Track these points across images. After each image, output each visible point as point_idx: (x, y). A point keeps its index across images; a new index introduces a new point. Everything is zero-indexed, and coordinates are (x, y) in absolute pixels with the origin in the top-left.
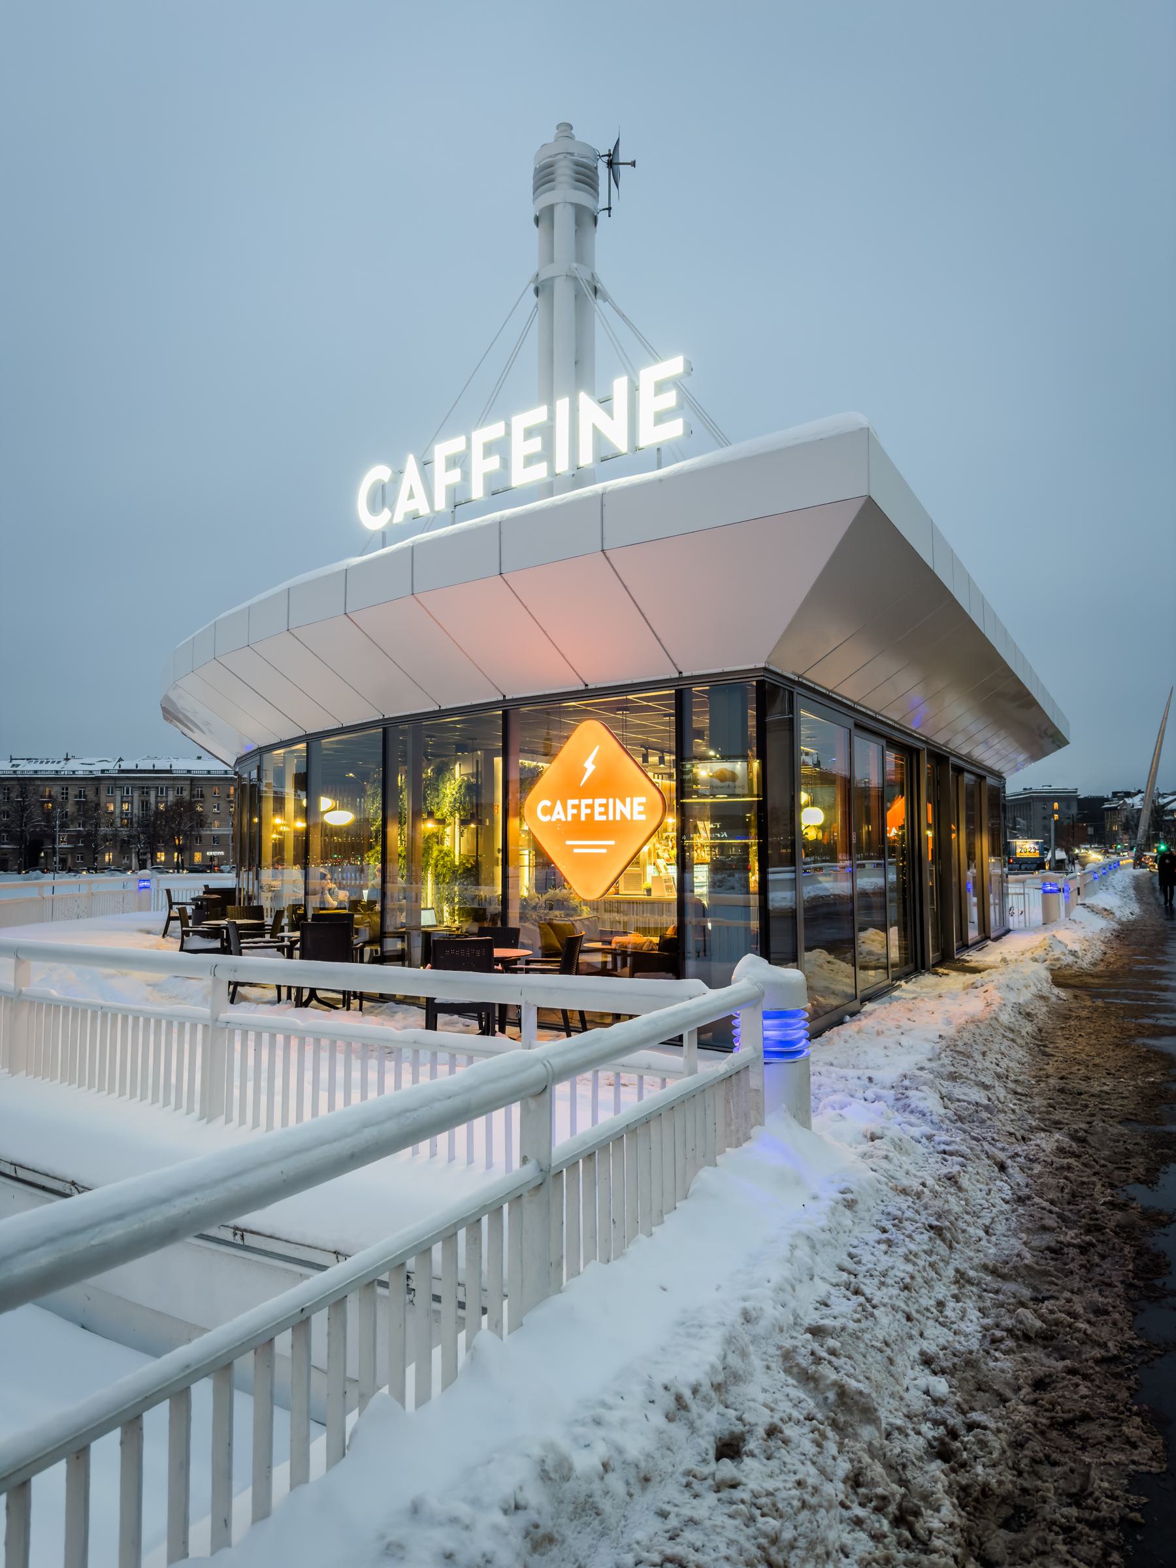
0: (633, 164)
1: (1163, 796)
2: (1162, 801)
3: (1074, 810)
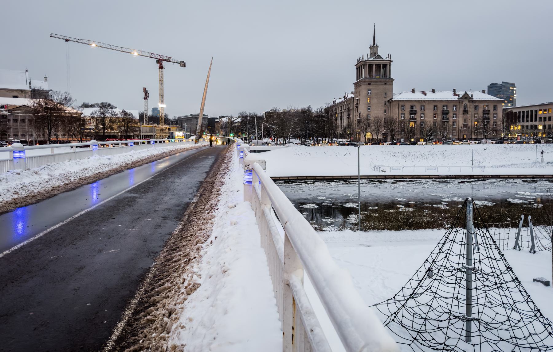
0: (183, 64)
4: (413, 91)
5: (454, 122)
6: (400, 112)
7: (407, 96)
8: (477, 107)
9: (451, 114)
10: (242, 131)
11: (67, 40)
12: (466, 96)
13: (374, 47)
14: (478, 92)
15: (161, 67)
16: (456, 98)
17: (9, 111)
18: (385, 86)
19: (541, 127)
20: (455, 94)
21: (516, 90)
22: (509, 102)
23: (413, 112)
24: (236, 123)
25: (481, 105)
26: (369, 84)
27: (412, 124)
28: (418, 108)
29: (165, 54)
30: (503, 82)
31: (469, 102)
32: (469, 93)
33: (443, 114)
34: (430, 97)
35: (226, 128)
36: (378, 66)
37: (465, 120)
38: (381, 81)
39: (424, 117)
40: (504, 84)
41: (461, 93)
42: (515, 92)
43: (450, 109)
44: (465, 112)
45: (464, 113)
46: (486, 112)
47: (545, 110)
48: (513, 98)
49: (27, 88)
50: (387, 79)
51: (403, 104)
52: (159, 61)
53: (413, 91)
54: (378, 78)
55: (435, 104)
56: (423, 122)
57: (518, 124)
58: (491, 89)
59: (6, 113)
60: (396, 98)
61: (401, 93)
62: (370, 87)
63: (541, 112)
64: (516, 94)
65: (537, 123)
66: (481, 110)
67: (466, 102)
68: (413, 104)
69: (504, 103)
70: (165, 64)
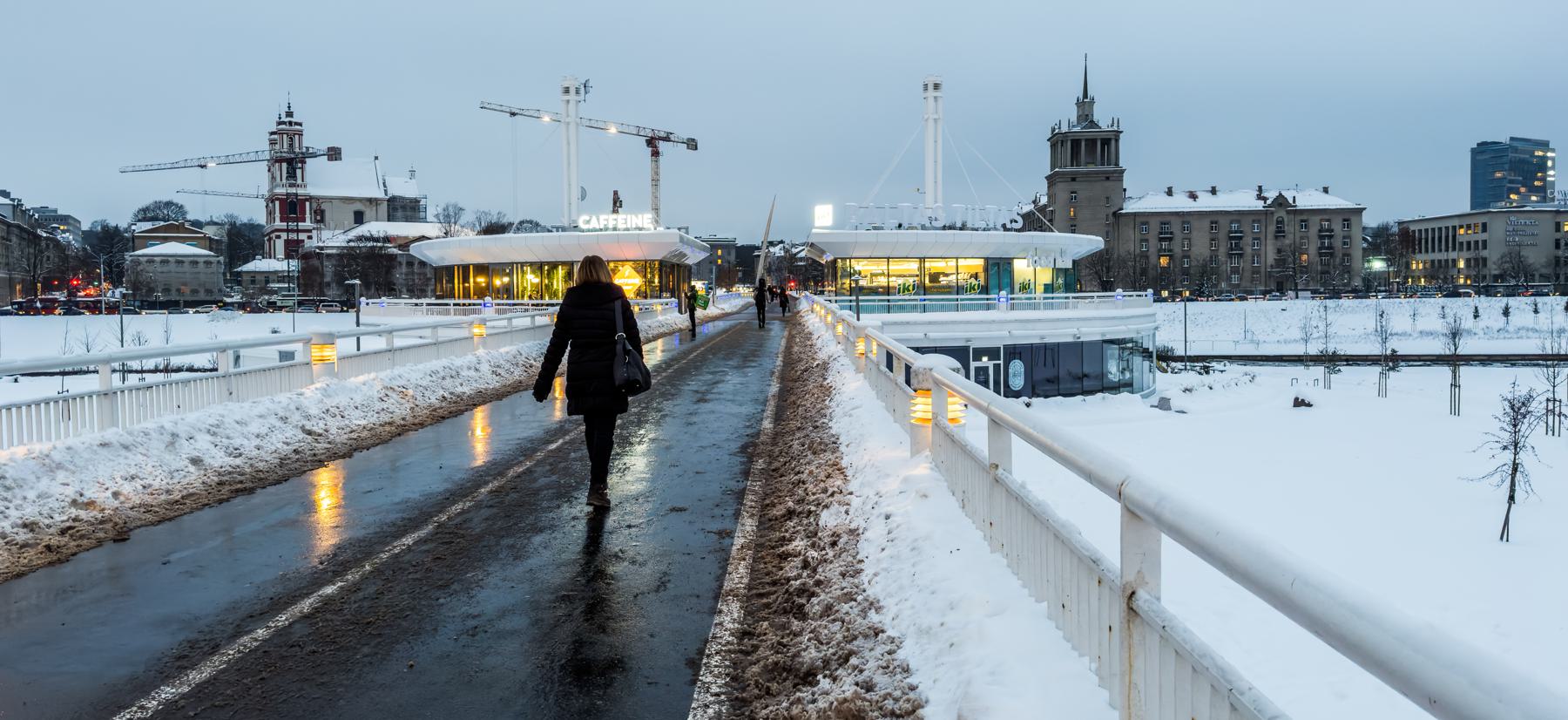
0: (692, 144)
1: (794, 246)
2: (794, 251)
3: (732, 258)
4: (1170, 192)
5: (1257, 254)
6: (1138, 236)
7: (1155, 203)
8: (1305, 224)
9: (1248, 240)
10: (814, 278)
11: (513, 114)
12: (1280, 201)
13: (1085, 104)
14: (1313, 192)
15: (656, 154)
16: (1260, 205)
17: (400, 247)
18: (1107, 184)
19: (1462, 264)
20: (1260, 197)
21: (1553, 159)
22: (1536, 190)
23: (1166, 237)
24: (801, 259)
25: (1316, 219)
26: (1074, 180)
27: (1164, 261)
28: (1176, 227)
29: (662, 128)
30: (1512, 139)
31: (1288, 212)
32: (1289, 195)
33: (1161, 240)
34: (1206, 203)
35: (779, 269)
36: (1091, 142)
37: (1279, 251)
38: (1097, 173)
39: (1190, 245)
40: (1515, 144)
41: (1271, 195)
42: (1550, 163)
43: (1246, 228)
44: (1280, 233)
45: (1276, 237)
46: (1326, 234)
47: (1469, 227)
48: (1543, 179)
49: (380, 194)
50: (1112, 168)
51: (1143, 219)
52: (651, 142)
53: (1170, 192)
54: (1092, 168)
55: (1214, 217)
56: (1186, 256)
57: (1418, 256)
58: (1479, 157)
59: (396, 251)
60: (1130, 207)
61: (1144, 195)
62: (1075, 186)
63: (1462, 231)
64: (1553, 168)
65: (1452, 255)
66: (1314, 231)
67: (1282, 213)
68: (1165, 218)
69: (1518, 193)
70: (662, 145)
